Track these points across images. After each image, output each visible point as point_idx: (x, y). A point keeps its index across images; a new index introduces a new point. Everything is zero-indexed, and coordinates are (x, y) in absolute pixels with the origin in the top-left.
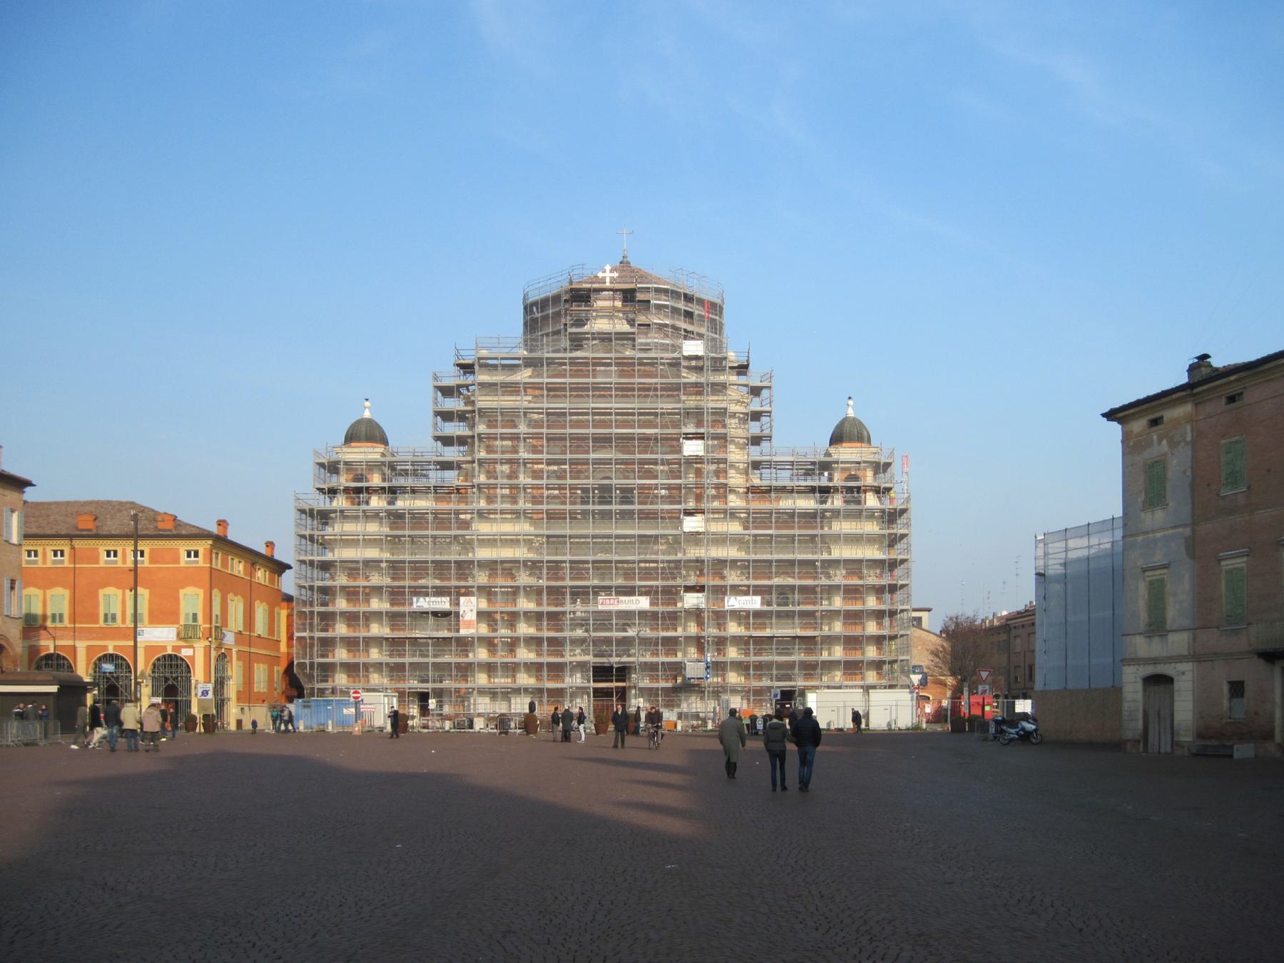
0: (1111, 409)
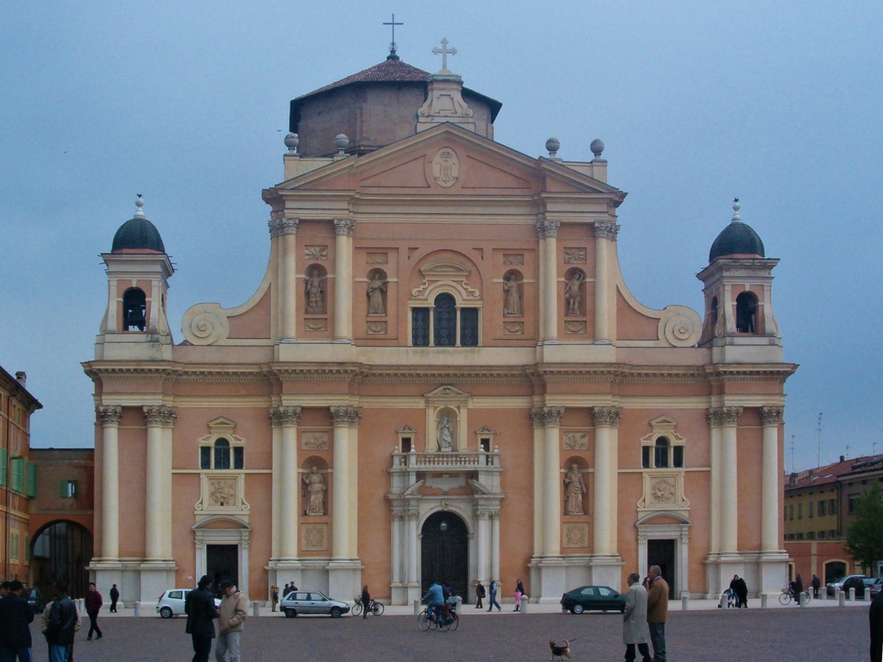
0: (832, 464)
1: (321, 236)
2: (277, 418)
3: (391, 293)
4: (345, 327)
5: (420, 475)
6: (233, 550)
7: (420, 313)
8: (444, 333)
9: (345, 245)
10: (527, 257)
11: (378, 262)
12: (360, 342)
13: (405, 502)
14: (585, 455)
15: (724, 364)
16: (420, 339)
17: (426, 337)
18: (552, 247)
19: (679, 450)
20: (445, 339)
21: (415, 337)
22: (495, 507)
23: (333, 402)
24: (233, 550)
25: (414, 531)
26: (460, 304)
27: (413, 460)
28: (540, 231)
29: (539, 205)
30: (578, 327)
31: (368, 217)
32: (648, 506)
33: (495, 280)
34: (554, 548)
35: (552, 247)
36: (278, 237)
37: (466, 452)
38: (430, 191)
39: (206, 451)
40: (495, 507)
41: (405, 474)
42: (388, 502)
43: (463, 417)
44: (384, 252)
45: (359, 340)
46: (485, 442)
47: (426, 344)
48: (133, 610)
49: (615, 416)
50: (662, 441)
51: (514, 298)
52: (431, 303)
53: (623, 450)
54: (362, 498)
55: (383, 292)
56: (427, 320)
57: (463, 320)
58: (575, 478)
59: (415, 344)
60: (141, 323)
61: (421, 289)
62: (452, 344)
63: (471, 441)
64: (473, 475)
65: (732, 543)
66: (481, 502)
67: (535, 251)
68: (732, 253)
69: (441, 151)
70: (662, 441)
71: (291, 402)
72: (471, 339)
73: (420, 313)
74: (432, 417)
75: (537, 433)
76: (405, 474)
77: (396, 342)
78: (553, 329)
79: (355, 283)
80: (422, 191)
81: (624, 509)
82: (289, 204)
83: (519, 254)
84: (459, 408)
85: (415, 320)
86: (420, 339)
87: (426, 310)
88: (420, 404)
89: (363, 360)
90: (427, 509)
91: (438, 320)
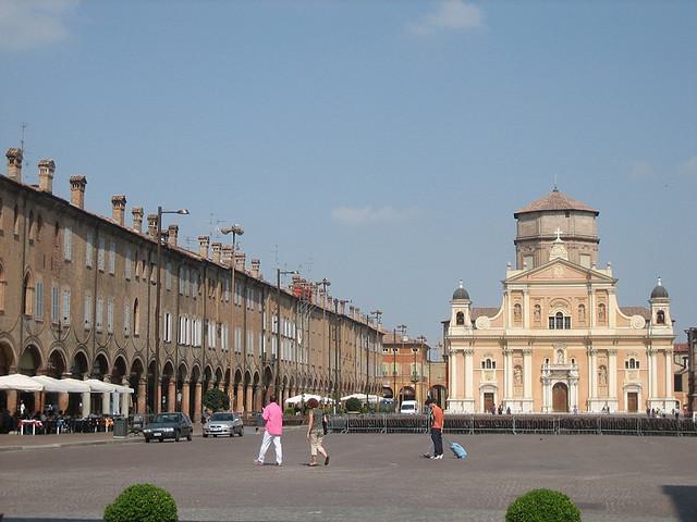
1: (604, 294)
2: (590, 353)
4: (527, 324)
6: (636, 394)
9: (527, 297)
11: (537, 302)
13: (546, 380)
14: (521, 364)
16: (551, 327)
19: (638, 363)
20: (560, 327)
23: (465, 348)
24: (636, 394)
25: (550, 388)
28: (590, 293)
29: (589, 284)
31: (532, 288)
32: (627, 381)
34: (595, 395)
39: (627, 363)
41: (547, 371)
42: (541, 380)
43: (565, 352)
49: (615, 352)
50: (632, 360)
53: (618, 362)
54: (533, 380)
60: (463, 323)
65: (655, 395)
70: (632, 360)
71: (595, 348)
72: (568, 327)
74: (555, 351)
76: (547, 371)
81: (619, 382)
83: (583, 299)
86: (551, 327)
87: (553, 318)
89: (533, 334)
90: (554, 382)
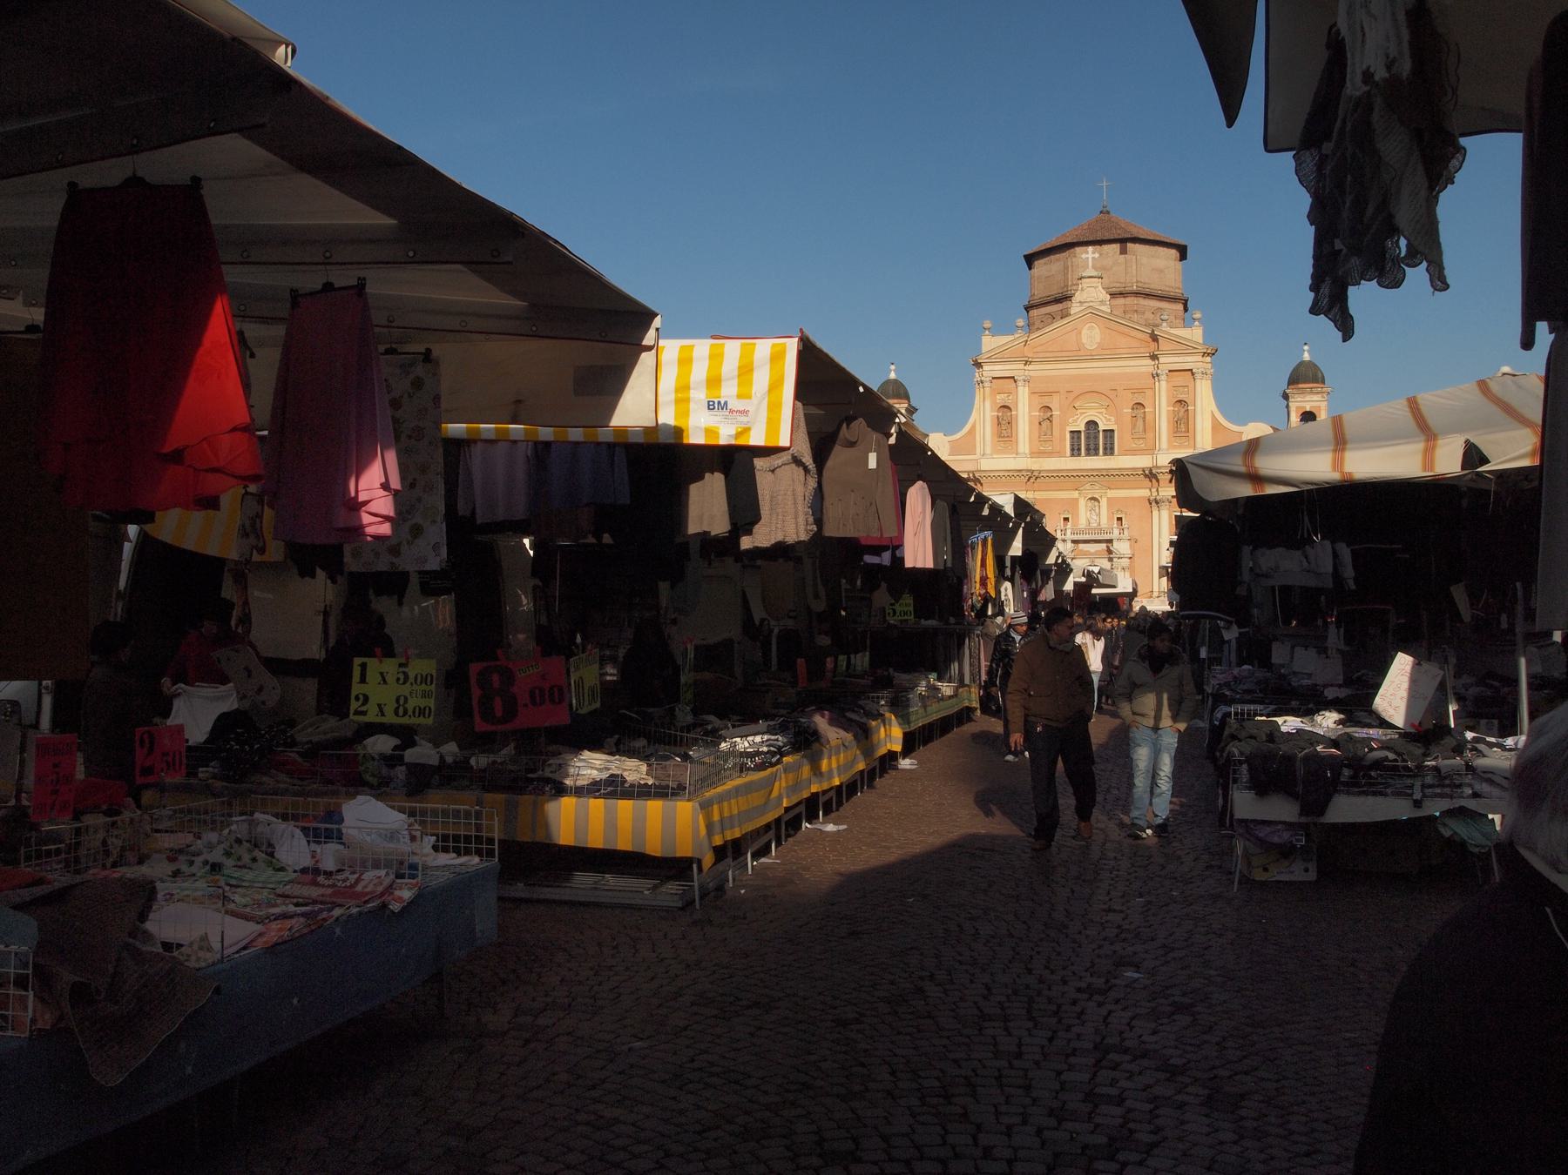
3: (1055, 421)
4: (1024, 444)
5: (1074, 542)
7: (1075, 434)
8: (1092, 447)
9: (1023, 393)
10: (1149, 393)
11: (1046, 401)
12: (1033, 455)
15: (1157, 467)
16: (1075, 451)
17: (1079, 449)
18: (1163, 386)
20: (1092, 451)
21: (1072, 450)
22: (1125, 562)
26: (1102, 427)
27: (1069, 532)
30: (1184, 439)
31: (1035, 370)
33: (1125, 411)
35: (1163, 386)
36: (1336, 451)
37: (1106, 526)
38: (1080, 353)
40: (1125, 562)
43: (1104, 502)
44: (1050, 394)
45: (1036, 454)
46: (1119, 519)
47: (1079, 455)
48: (1419, 446)
51: (1140, 423)
52: (1082, 428)
55: (1050, 419)
56: (1079, 438)
57: (1105, 437)
58: (311, 901)
59: (1072, 455)
61: (1075, 418)
62: (1097, 454)
63: (1110, 519)
64: (1110, 541)
66: (1115, 560)
67: (1153, 389)
68: (1298, 383)
69: (1089, 325)
72: (1109, 450)
73: (1075, 434)
75: (1155, 513)
77: (1060, 454)
78: (1164, 445)
79: (1031, 416)
80: (1075, 353)
82: (985, 368)
83: (1141, 391)
84: (1101, 497)
85: (1072, 438)
86: (1075, 451)
88: (1075, 494)
91: (1087, 438)
